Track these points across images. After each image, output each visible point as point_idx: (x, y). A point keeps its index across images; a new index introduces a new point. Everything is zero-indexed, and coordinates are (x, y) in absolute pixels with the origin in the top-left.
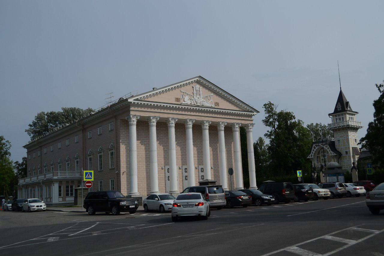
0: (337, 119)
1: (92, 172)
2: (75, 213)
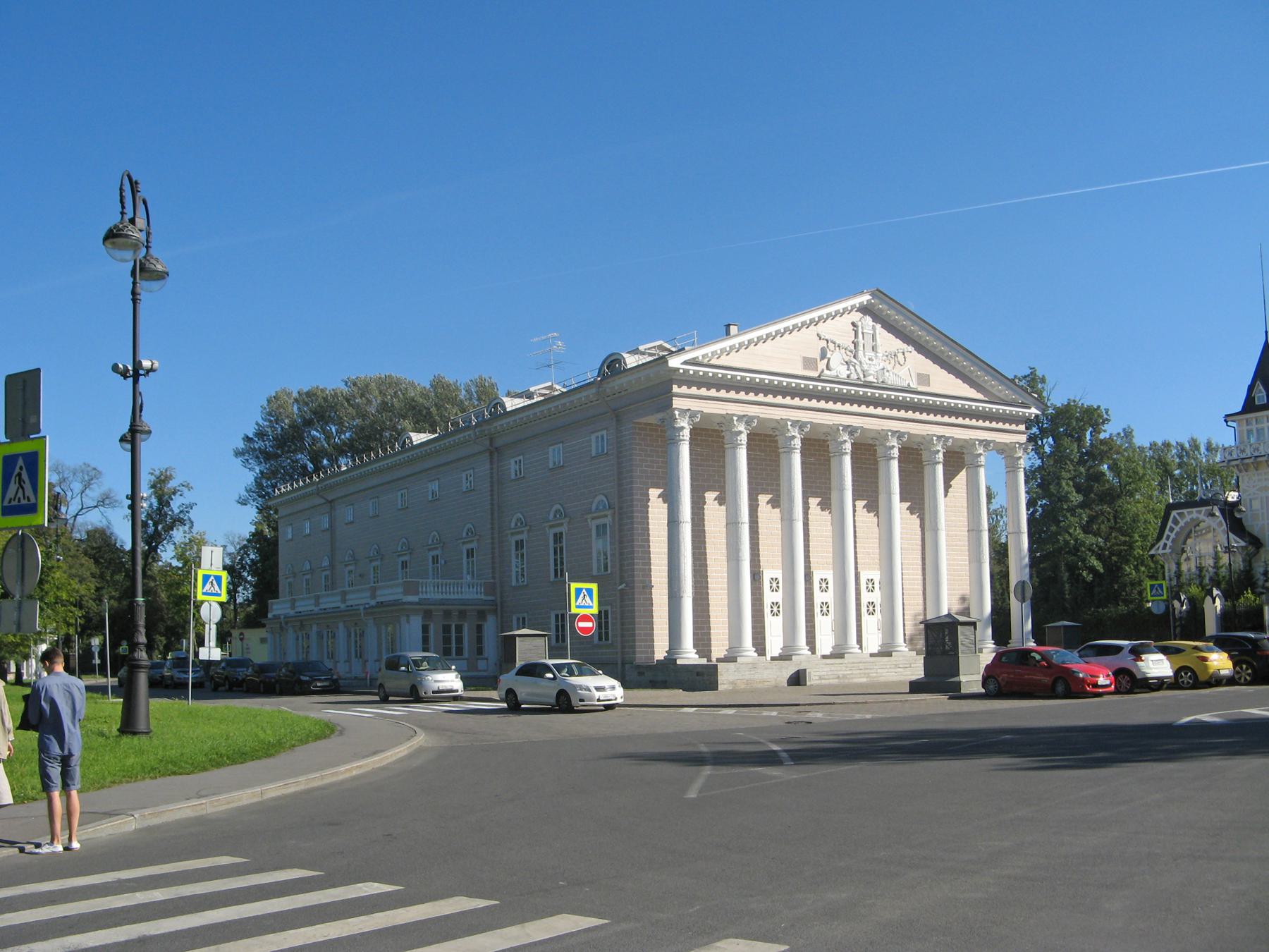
0: (1249, 432)
1: (594, 587)
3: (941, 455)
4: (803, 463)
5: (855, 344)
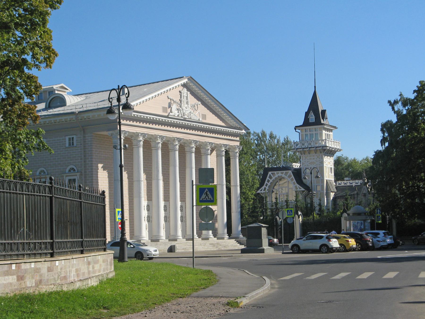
2: (311, 248)
3: (194, 149)
4: (143, 151)
5: (181, 101)
